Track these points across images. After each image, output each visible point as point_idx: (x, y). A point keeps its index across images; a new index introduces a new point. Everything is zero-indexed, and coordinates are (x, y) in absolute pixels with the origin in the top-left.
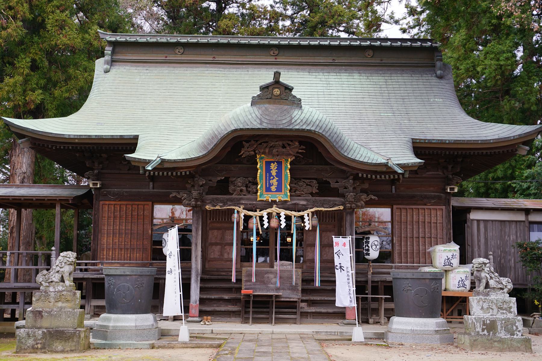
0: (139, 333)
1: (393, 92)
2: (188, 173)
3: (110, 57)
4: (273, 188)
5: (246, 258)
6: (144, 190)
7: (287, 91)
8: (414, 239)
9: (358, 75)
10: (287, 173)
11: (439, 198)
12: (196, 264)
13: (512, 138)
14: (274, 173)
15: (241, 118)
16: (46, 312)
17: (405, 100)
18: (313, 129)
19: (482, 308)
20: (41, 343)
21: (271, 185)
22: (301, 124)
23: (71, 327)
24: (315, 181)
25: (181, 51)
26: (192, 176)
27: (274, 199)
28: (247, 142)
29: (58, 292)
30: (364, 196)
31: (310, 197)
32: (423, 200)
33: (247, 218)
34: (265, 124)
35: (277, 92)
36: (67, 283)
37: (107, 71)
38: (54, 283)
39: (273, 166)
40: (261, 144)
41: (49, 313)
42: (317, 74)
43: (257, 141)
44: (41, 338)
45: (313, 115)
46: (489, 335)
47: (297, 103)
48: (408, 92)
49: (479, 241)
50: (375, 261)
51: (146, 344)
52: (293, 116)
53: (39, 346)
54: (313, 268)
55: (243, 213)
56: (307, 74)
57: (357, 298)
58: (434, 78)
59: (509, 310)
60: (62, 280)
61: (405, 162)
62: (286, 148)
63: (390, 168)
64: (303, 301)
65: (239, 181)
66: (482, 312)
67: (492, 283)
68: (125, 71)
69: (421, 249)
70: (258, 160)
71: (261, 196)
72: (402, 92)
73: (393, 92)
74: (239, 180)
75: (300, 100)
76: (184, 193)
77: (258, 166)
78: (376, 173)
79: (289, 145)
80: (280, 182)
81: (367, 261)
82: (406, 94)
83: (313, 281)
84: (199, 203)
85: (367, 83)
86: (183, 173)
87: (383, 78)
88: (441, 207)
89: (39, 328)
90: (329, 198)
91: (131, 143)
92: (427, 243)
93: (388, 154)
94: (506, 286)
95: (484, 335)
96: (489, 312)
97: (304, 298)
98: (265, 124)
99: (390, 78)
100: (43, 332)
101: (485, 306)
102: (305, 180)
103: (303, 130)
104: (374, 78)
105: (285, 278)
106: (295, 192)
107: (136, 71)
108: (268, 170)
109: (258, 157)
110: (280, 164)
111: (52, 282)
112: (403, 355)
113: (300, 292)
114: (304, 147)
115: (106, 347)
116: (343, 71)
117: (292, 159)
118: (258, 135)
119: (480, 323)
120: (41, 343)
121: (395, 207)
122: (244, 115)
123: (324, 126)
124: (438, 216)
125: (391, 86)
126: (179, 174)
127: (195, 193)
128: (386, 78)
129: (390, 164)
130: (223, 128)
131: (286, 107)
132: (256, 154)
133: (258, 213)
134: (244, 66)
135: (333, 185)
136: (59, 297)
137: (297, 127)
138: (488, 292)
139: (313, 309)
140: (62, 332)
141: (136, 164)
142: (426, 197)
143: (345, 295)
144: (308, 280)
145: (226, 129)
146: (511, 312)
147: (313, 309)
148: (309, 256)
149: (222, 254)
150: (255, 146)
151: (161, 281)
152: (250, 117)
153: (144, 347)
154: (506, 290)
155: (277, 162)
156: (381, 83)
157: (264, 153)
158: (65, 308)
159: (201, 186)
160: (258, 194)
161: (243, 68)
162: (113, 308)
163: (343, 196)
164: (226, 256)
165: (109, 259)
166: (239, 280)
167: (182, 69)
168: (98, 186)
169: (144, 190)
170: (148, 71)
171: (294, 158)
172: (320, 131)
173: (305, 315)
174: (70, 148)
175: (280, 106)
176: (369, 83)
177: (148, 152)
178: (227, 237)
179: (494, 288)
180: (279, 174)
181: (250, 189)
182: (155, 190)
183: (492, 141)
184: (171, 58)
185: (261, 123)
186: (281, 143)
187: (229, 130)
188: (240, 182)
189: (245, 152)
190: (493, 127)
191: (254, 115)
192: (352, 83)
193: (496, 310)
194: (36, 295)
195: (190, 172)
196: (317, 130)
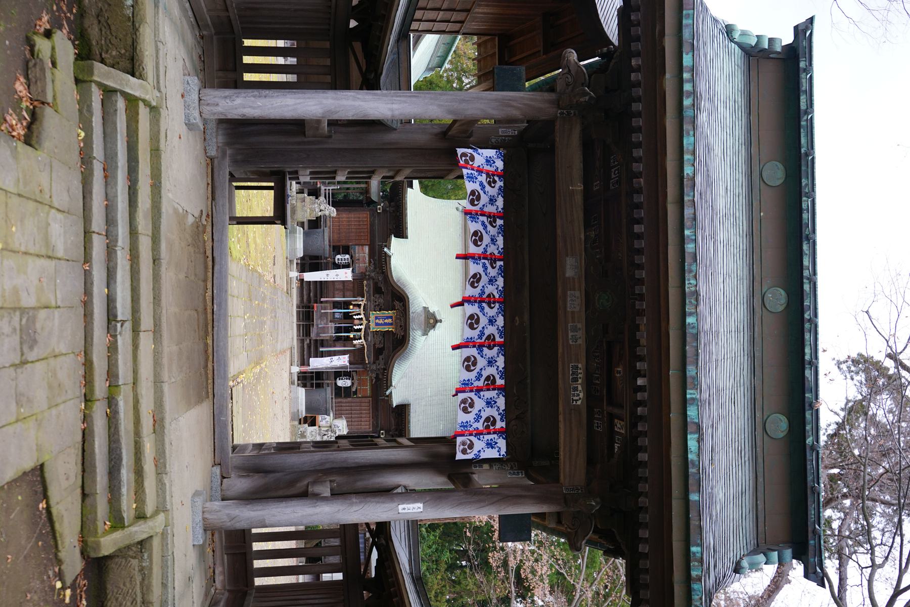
0: (294, 250)
4: (377, 321)
5: (336, 305)
11: (377, 426)
14: (386, 321)
26: (383, 273)
27: (371, 321)
32: (375, 416)
33: (359, 306)
35: (432, 321)
37: (457, 209)
39: (390, 321)
47: (425, 333)
50: (336, 384)
54: (331, 347)
55: (362, 303)
57: (312, 373)
65: (381, 301)
80: (381, 324)
81: (336, 379)
83: (322, 346)
91: (401, 233)
105: (324, 330)
108: (388, 318)
110: (391, 324)
127: (373, 274)
133: (362, 312)
135: (381, 357)
136: (312, 210)
139: (305, 347)
142: (377, 418)
143: (317, 363)
144: (323, 343)
147: (305, 347)
149: (338, 290)
162: (306, 235)
163: (374, 363)
164: (336, 292)
166: (322, 302)
173: (302, 341)
178: (348, 293)
180: (385, 324)
189: (397, 303)
194: (313, 198)
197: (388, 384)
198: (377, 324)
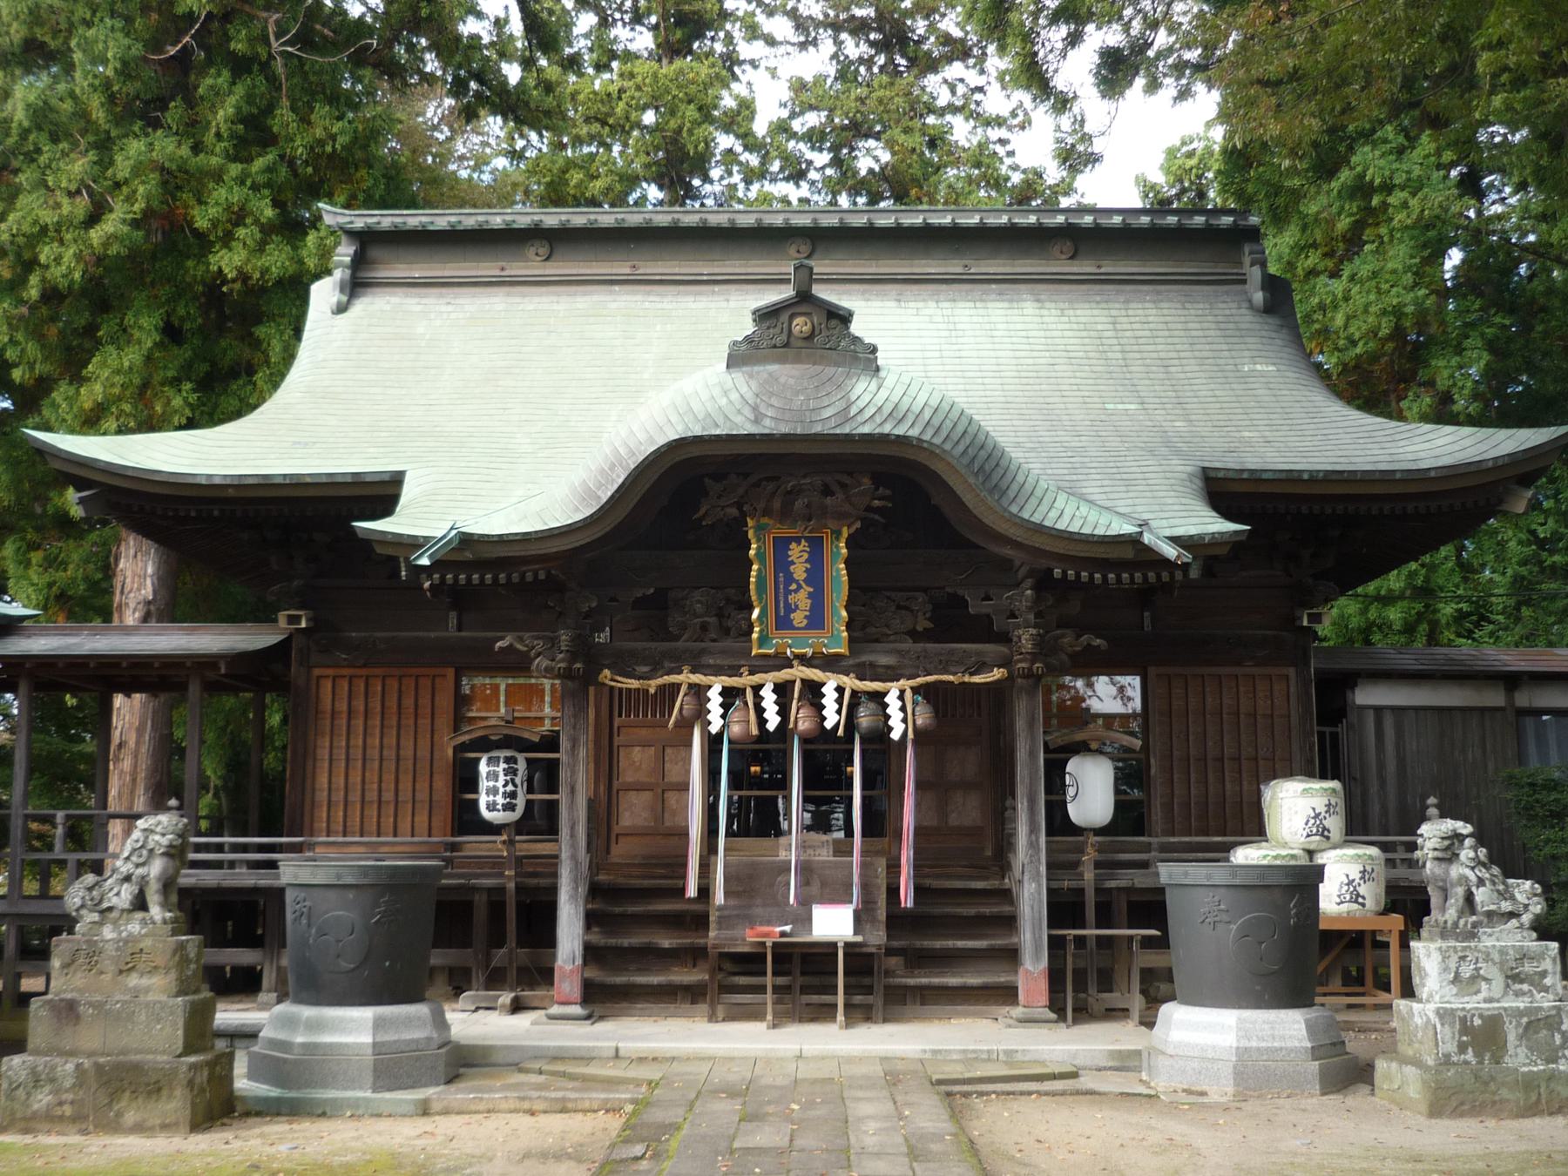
1: (1135, 348)
2: (542, 576)
3: (348, 272)
4: (799, 618)
6: (433, 635)
7: (834, 322)
8: (1261, 762)
9: (1036, 305)
10: (838, 570)
12: (574, 846)
13: (1490, 464)
14: (799, 571)
15: (696, 407)
16: (91, 1004)
17: (1173, 369)
18: (914, 432)
19: (1457, 979)
20: (72, 1103)
21: (790, 609)
22: (878, 419)
23: (164, 1052)
24: (921, 597)
25: (541, 251)
27: (803, 656)
28: (718, 478)
29: (126, 942)
30: (1068, 639)
31: (908, 645)
34: (767, 422)
35: (800, 325)
36: (156, 912)
37: (341, 309)
38: (114, 914)
39: (798, 554)
40: (757, 485)
41: (98, 1006)
42: (921, 305)
43: (746, 475)
44: (74, 1085)
45: (912, 392)
46: (1481, 1062)
47: (865, 358)
48: (1179, 347)
49: (1381, 766)
51: (405, 1101)
52: (853, 398)
53: (68, 1110)
56: (893, 304)
58: (1244, 311)
59: (1537, 981)
60: (140, 904)
61: (1193, 531)
62: (832, 494)
63: (1148, 549)
64: (890, 952)
66: (1455, 990)
67: (1480, 895)
68: (388, 307)
69: (1228, 793)
70: (751, 534)
71: (763, 641)
72: (1160, 347)
73: (1135, 348)
74: (697, 595)
75: (873, 350)
76: (538, 638)
77: (752, 552)
78: (1105, 564)
79: (843, 486)
82: (1174, 355)
84: (578, 665)
85: (1060, 326)
86: (529, 577)
87: (1106, 312)
88: (1284, 671)
89: (72, 1053)
90: (964, 646)
91: (382, 494)
92: (1244, 775)
93: (1139, 509)
94: (1526, 906)
95: (1466, 1063)
96: (1478, 992)
97: (895, 944)
98: (767, 422)
99: (1123, 312)
100: (78, 1066)
101: (1467, 971)
102: (893, 595)
103: (884, 438)
104: (1079, 312)
106: (864, 628)
107: (419, 308)
109: (750, 523)
110: (816, 546)
111: (110, 909)
112: (1174, 1097)
113: (883, 927)
114: (888, 492)
115: (284, 1110)
116: (993, 296)
117: (852, 530)
118: (754, 455)
119: (1452, 1025)
120: (72, 1103)
121: (1152, 671)
122: (705, 396)
123: (948, 424)
124: (1283, 695)
125: (1128, 334)
126: (515, 577)
128: (1113, 312)
129: (1147, 538)
130: (642, 436)
131: (830, 371)
132: (744, 515)
134: (717, 288)
137: (866, 429)
138: (1475, 925)
140: (136, 1068)
141: (390, 551)
145: (651, 440)
146: (1546, 989)
148: (673, 775)
150: (741, 491)
151: (477, 897)
152: (723, 401)
153: (400, 1110)
154: (1526, 918)
155: (807, 539)
156: (1100, 327)
157: (767, 512)
158: (147, 990)
159: (587, 616)
160: (755, 636)
161: (713, 292)
163: (1005, 638)
165: (336, 834)
167: (544, 299)
168: (303, 625)
169: (433, 635)
170: (450, 308)
171: (858, 525)
172: (937, 441)
174: (216, 513)
175: (813, 369)
176: (1067, 326)
177: (424, 517)
179: (1490, 914)
180: (816, 577)
181: (730, 623)
182: (463, 634)
183: (1433, 474)
184: (516, 269)
185: (758, 418)
186: (817, 480)
187: (661, 441)
188: (699, 602)
190: (1431, 436)
191: (734, 396)
192: (1019, 327)
193: (1498, 983)
194: (61, 946)
195: (548, 574)
196: (927, 437)
197: (1130, 553)
198: (816, 620)
